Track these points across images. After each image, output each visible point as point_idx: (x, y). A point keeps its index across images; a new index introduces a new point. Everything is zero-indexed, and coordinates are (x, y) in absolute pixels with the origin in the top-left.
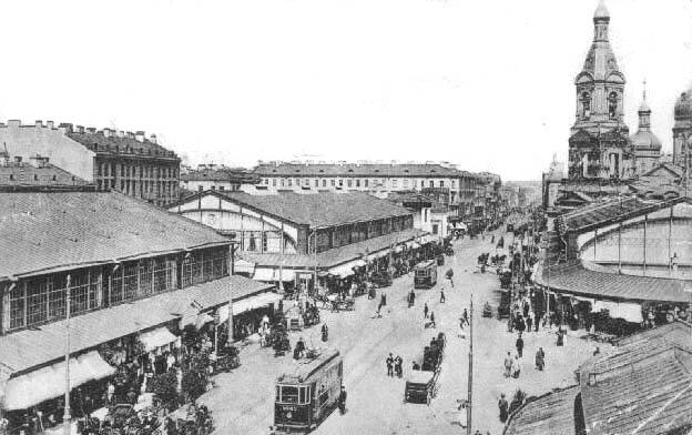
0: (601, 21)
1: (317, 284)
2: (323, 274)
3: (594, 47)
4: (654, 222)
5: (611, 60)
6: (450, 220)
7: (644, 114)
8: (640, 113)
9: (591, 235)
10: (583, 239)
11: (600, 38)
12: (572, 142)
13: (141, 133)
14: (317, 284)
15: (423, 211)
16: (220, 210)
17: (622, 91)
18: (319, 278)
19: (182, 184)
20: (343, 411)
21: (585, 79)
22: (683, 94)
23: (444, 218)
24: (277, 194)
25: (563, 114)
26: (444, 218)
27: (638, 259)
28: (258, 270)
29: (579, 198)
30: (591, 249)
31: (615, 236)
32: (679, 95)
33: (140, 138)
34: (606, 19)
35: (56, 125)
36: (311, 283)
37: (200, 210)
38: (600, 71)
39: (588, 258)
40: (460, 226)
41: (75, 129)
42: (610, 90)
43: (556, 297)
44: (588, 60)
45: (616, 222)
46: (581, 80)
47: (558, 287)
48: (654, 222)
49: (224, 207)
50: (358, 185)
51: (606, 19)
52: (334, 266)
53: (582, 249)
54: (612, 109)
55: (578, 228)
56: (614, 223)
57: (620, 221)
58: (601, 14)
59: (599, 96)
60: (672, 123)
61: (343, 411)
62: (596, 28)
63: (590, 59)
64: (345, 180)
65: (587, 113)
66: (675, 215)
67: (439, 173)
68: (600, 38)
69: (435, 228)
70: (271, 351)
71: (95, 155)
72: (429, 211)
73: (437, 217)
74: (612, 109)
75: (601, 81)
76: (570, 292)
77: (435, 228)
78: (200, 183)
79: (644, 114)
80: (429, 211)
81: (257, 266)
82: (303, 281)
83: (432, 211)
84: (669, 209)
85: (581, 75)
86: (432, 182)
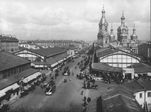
6: (74, 51)
7: (112, 30)
9: (102, 57)
10: (101, 58)
12: (98, 36)
13: (10, 35)
16: (104, 58)
17: (108, 26)
18: (49, 67)
20: (81, 94)
21: (100, 24)
23: (73, 51)
26: (73, 51)
27: (123, 56)
30: (102, 60)
31: (107, 57)
32: (118, 27)
33: (10, 36)
34: (104, 12)
38: (103, 22)
39: (101, 61)
47: (51, 55)
54: (106, 30)
55: (100, 54)
58: (103, 11)
59: (103, 28)
61: (81, 94)
64: (53, 43)
73: (72, 51)
74: (106, 30)
78: (23, 45)
79: (112, 30)
81: (35, 65)
82: (45, 68)
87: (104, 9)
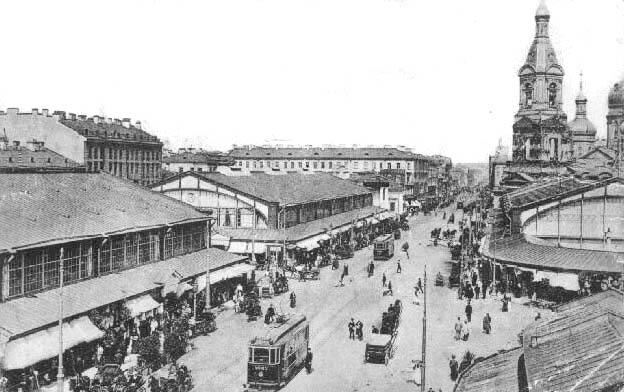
0: (542, 19)
1: (286, 256)
2: (291, 247)
3: (536, 42)
4: (590, 200)
5: (551, 54)
6: (406, 198)
7: (581, 102)
8: (577, 102)
9: (533, 212)
10: (525, 215)
11: (541, 35)
12: (516, 128)
13: (127, 120)
14: (286, 256)
15: (382, 190)
16: (199, 190)
17: (561, 82)
18: (288, 250)
20: (309, 370)
21: (527, 71)
23: (400, 196)
24: (249, 174)
25: (508, 103)
26: (400, 196)
28: (233, 244)
30: (533, 224)
31: (555, 213)
32: (612, 86)
33: (126, 125)
34: (547, 18)
35: (51, 113)
36: (281, 255)
37: (181, 189)
38: (541, 64)
39: (530, 232)
40: (415, 204)
41: (68, 116)
42: (550, 81)
43: (501, 267)
44: (530, 54)
45: (556, 200)
46: (524, 72)
48: (590, 200)
49: (202, 187)
51: (547, 18)
52: (301, 240)
53: (525, 225)
54: (552, 98)
55: (522, 205)
56: (553, 201)
57: (559, 199)
58: (542, 13)
59: (541, 87)
60: (606, 111)
61: (309, 370)
62: (538, 25)
63: (532, 53)
64: (311, 162)
65: (530, 102)
66: (609, 194)
67: (395, 156)
68: (541, 35)
69: (392, 205)
70: (245, 316)
71: (86, 139)
72: (386, 190)
73: (394, 195)
74: (552, 98)
75: (542, 73)
76: (514, 263)
77: (392, 205)
78: (181, 165)
79: (581, 102)
80: (386, 190)
81: (231, 240)
82: (273, 253)
83: (389, 190)
84: (603, 188)
85: (524, 67)
86: (389, 164)
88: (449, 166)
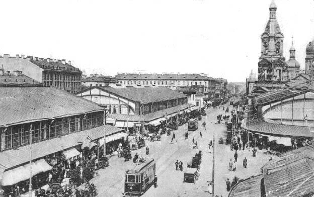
0: (273, 10)
1: (144, 129)
2: (147, 124)
3: (270, 21)
4: (297, 100)
5: (277, 27)
6: (204, 99)
7: (292, 51)
8: (291, 51)
9: (268, 106)
10: (264, 108)
11: (272, 17)
12: (259, 64)
13: (64, 60)
14: (144, 129)
15: (192, 96)
17: (282, 41)
18: (145, 126)
19: (83, 83)
20: (156, 186)
21: (265, 36)
22: (310, 43)
23: (201, 99)
25: (255, 52)
26: (201, 99)
28: (117, 122)
29: (263, 90)
30: (268, 113)
31: (279, 107)
32: (308, 43)
33: (64, 63)
34: (275, 9)
35: (25, 57)
36: (141, 128)
37: (91, 95)
38: (272, 32)
39: (267, 117)
40: (209, 102)
41: (34, 58)
42: (277, 41)
44: (267, 27)
45: (280, 101)
46: (264, 36)
48: (297, 100)
49: (101, 94)
50: (163, 84)
51: (275, 9)
52: (152, 121)
53: (264, 113)
54: (278, 49)
55: (262, 103)
56: (278, 101)
57: (281, 100)
58: (273, 7)
59: (272, 44)
60: (305, 56)
61: (156, 186)
62: (271, 13)
63: (268, 27)
64: (157, 82)
65: (267, 51)
66: (306, 97)
67: (199, 78)
68: (272, 17)
69: (197, 103)
70: (123, 159)
72: (194, 96)
73: (198, 98)
74: (278, 49)
75: (273, 37)
76: (259, 132)
77: (197, 103)
78: (91, 83)
79: (292, 51)
80: (194, 96)
81: (116, 121)
82: (137, 127)
83: (196, 96)
84: (304, 95)
85: (264, 34)
86: (196, 82)
87: (294, 46)
88: (226, 83)
